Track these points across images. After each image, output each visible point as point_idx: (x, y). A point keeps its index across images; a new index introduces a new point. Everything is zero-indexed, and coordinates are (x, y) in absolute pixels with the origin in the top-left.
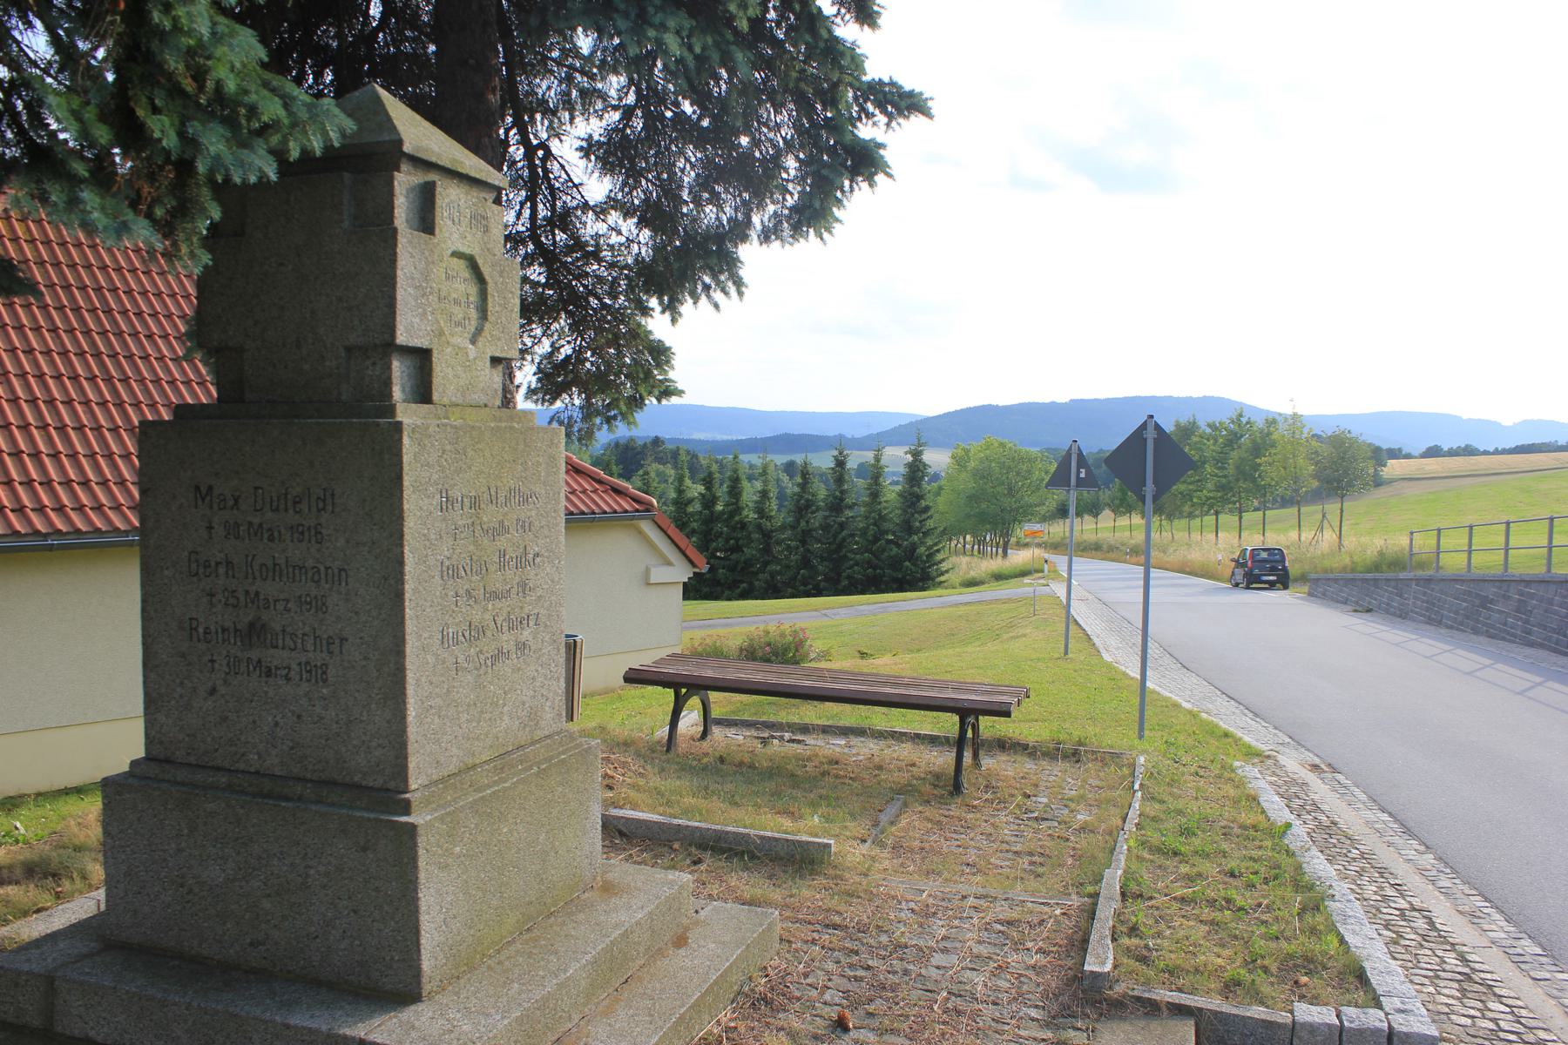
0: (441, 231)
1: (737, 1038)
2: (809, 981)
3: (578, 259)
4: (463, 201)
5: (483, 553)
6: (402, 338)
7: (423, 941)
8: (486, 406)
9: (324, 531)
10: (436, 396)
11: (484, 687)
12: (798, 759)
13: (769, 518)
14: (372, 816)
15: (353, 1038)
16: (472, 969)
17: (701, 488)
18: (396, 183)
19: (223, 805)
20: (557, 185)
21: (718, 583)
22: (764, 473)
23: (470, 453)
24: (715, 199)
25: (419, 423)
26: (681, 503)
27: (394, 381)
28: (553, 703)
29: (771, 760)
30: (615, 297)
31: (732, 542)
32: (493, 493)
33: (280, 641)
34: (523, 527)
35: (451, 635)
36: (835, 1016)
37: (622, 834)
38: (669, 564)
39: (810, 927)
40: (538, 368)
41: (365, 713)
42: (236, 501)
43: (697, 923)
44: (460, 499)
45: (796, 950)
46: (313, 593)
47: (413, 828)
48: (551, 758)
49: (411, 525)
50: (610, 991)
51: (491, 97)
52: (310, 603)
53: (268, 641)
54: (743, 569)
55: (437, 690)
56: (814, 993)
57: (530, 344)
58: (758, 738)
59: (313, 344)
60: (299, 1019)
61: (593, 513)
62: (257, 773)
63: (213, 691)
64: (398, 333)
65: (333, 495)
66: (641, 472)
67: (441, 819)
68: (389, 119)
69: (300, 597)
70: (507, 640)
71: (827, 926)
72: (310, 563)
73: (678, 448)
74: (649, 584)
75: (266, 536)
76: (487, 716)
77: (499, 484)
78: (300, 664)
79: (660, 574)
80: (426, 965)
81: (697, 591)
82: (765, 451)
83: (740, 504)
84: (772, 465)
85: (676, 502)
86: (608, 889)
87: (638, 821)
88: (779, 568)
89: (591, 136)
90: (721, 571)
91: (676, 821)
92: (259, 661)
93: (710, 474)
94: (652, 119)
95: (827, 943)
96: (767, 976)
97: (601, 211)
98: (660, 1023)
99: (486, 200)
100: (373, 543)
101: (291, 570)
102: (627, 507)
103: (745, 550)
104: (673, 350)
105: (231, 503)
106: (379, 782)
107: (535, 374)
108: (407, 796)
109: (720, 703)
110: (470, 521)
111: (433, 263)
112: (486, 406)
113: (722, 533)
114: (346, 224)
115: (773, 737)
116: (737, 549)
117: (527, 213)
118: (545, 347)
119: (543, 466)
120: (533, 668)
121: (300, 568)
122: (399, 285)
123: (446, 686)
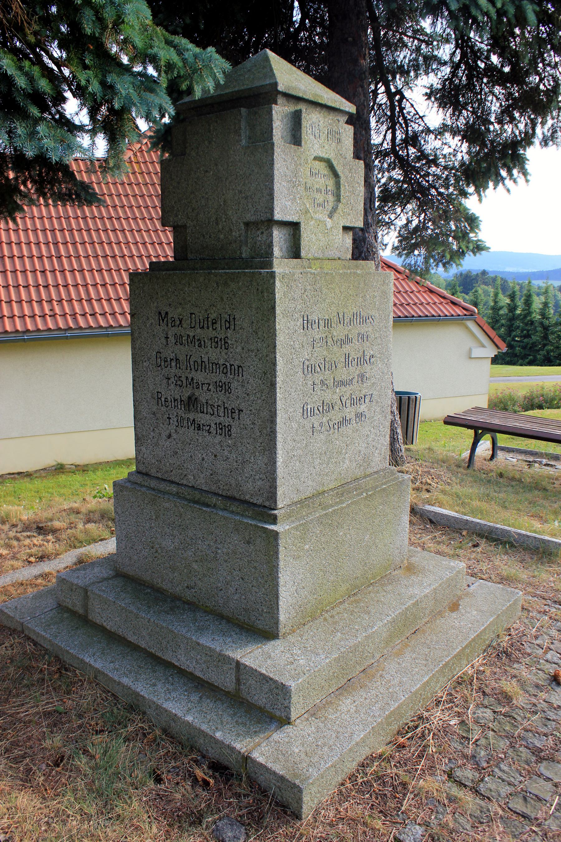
0: (306, 143)
1: (484, 679)
2: (538, 642)
3: (423, 165)
4: (321, 122)
5: (333, 356)
6: (278, 216)
7: (281, 603)
8: (339, 259)
9: (229, 342)
10: (303, 254)
11: (332, 442)
12: (549, 478)
13: (548, 318)
14: (253, 523)
15: (233, 659)
16: (314, 619)
17: (508, 301)
18: (274, 112)
19: (173, 505)
20: (409, 117)
21: (516, 355)
22: (546, 292)
23: (325, 291)
24: (512, 119)
25: (287, 272)
26: (496, 309)
27: (275, 244)
28: (381, 450)
29: (532, 477)
30: (447, 188)
31: (525, 332)
32: (341, 317)
33: (205, 409)
34: (362, 338)
35: (309, 410)
36: (552, 671)
37: (431, 522)
38: (483, 346)
39: (543, 601)
40: (399, 233)
41: (252, 458)
42: (181, 321)
43: (467, 594)
44: (317, 321)
45: (532, 618)
46: (223, 381)
47: (276, 534)
48: (377, 487)
49: (281, 339)
50: (403, 638)
51: (362, 61)
52: (222, 387)
53: (199, 409)
54: (531, 348)
55: (299, 445)
56: (540, 652)
57: (393, 219)
58: (526, 461)
59: (225, 221)
60: (205, 641)
61: (440, 316)
62: (193, 487)
63: (169, 436)
64: (276, 212)
65: (234, 319)
66: (473, 291)
67: (296, 528)
68: (271, 70)
69: (216, 382)
70: (350, 412)
71: (555, 602)
72: (221, 362)
73: (496, 277)
74: (471, 358)
75: (197, 343)
76: (334, 460)
77: (345, 310)
78: (216, 424)
79: (478, 352)
80: (282, 617)
81: (503, 359)
82: (548, 278)
83: (531, 310)
84: (551, 288)
85: (493, 308)
86: (411, 569)
87: (442, 515)
88: (552, 348)
89: (432, 85)
90: (517, 348)
91: (465, 518)
92: (194, 420)
93: (514, 292)
94: (472, 70)
95: (553, 615)
96: (510, 635)
97: (440, 132)
98: (432, 667)
99: (339, 121)
100: (258, 350)
101: (211, 365)
102: (460, 313)
103: (533, 337)
104: (480, 219)
105: (178, 322)
106: (259, 502)
107: (397, 237)
108: (276, 512)
109: (503, 440)
110: (324, 336)
111: (300, 164)
112: (339, 259)
113: (519, 327)
114: (244, 142)
115: (535, 462)
116: (528, 336)
117: (389, 136)
118: (402, 221)
119: (378, 298)
120: (367, 429)
121: (216, 365)
122: (275, 181)
123: (305, 442)
